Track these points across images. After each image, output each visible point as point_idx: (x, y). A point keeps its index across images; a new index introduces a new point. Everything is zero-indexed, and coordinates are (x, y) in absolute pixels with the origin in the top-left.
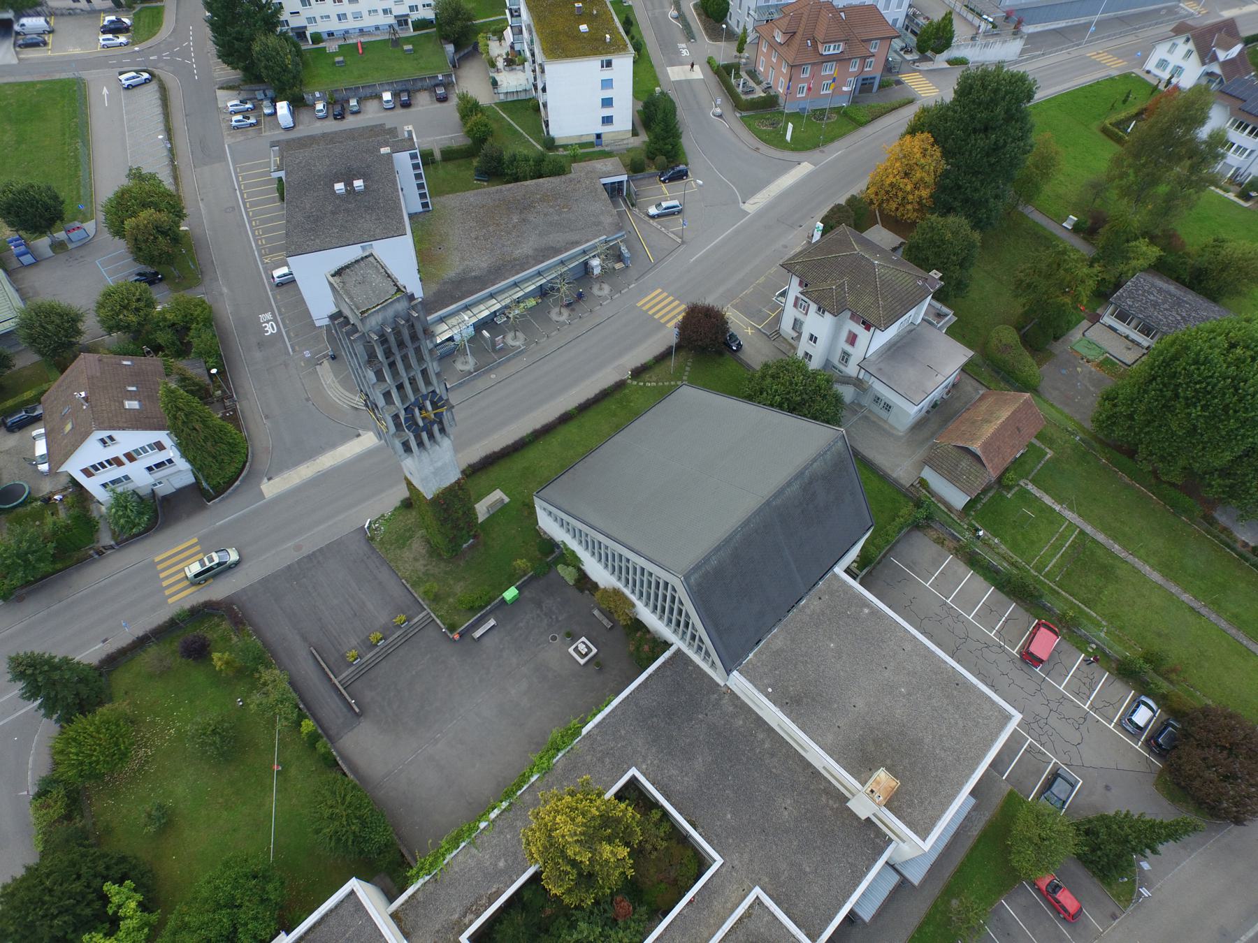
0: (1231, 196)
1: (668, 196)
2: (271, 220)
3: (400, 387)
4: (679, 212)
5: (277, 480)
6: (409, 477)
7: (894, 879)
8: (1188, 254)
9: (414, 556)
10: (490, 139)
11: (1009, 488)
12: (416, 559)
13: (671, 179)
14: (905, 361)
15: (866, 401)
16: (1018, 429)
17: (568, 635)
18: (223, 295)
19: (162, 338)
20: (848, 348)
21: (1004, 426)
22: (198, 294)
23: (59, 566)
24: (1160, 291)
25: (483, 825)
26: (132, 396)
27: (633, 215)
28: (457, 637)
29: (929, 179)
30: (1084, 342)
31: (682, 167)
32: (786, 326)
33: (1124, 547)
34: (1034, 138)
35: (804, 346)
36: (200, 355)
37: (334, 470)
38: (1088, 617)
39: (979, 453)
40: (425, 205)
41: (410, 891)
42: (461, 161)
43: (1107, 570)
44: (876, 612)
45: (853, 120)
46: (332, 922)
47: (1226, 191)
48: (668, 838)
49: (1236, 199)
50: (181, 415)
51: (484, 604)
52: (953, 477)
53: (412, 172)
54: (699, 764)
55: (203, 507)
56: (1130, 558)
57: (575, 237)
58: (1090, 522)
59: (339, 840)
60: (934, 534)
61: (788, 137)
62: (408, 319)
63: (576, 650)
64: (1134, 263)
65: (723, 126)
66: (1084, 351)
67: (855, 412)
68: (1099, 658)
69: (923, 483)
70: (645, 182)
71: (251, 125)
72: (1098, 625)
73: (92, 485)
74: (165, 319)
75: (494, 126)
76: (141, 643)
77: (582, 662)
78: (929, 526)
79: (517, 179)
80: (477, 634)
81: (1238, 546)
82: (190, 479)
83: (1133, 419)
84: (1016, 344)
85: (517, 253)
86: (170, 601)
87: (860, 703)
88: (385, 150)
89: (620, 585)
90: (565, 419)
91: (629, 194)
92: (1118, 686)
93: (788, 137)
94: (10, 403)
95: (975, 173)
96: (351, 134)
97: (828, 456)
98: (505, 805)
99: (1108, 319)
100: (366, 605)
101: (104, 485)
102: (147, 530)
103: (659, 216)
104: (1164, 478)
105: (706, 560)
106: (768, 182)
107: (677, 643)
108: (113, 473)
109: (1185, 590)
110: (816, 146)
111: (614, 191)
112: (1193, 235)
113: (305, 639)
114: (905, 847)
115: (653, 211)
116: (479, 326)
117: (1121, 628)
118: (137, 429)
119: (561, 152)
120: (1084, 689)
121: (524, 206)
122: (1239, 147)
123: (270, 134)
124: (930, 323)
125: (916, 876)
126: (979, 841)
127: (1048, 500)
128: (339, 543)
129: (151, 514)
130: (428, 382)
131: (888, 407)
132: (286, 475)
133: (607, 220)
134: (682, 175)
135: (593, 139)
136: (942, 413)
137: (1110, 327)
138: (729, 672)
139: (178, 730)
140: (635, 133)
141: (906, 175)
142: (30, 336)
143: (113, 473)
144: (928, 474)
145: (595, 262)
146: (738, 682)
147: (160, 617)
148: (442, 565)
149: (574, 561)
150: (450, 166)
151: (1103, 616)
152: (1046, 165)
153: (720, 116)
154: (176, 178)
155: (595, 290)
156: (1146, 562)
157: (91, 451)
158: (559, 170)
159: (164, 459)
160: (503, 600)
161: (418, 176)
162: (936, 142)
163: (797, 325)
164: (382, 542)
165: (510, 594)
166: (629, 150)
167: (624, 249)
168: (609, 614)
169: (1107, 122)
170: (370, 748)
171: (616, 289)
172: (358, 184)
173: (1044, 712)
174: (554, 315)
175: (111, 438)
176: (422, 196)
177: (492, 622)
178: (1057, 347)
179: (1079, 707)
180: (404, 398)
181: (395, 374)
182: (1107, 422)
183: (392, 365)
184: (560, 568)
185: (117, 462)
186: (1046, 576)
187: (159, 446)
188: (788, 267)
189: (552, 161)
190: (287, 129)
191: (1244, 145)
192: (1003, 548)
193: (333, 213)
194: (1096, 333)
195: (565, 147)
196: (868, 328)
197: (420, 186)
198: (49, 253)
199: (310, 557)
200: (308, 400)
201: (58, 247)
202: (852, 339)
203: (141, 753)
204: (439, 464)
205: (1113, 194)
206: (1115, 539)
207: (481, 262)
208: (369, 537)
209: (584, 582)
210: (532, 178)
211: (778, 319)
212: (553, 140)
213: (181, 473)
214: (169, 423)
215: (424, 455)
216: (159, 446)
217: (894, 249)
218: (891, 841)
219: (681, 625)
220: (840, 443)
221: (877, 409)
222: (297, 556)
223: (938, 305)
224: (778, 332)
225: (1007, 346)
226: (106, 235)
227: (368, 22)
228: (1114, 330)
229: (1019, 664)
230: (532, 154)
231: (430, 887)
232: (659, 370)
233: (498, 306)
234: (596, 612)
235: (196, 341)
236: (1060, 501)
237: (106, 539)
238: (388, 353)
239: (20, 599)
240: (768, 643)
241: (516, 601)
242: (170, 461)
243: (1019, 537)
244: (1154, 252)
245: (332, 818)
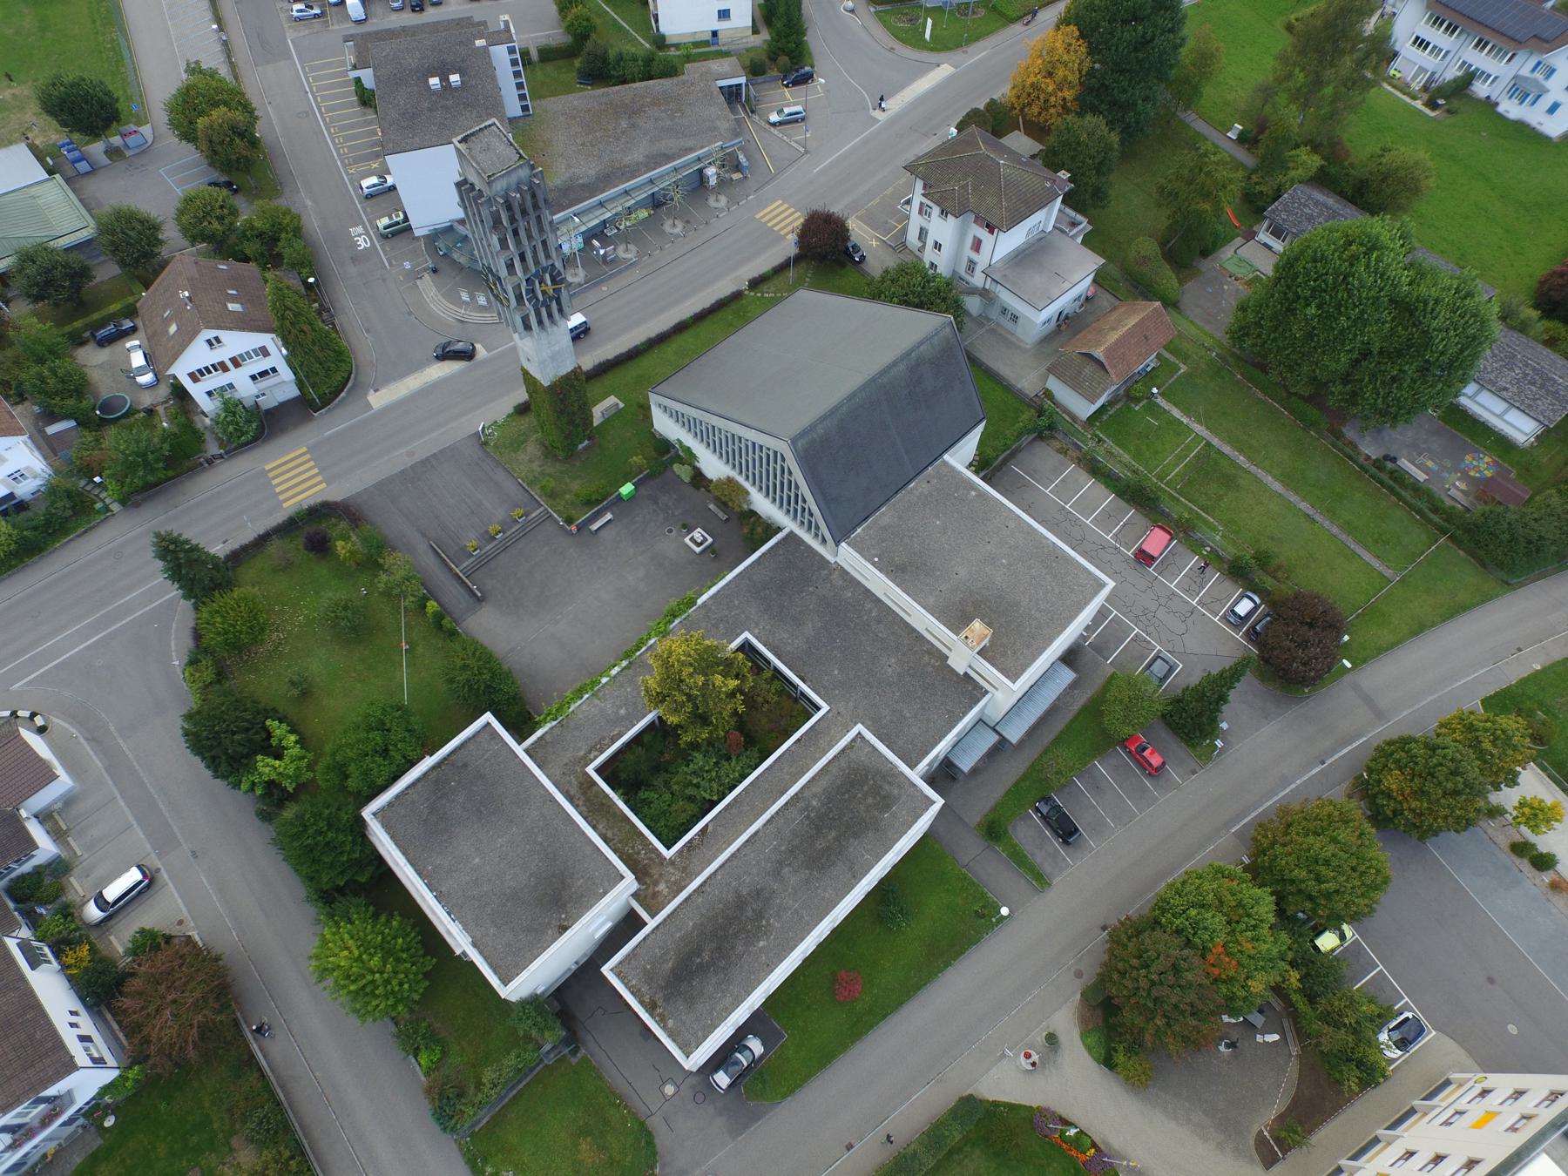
0: (1418, 104)
1: (791, 101)
2: (352, 126)
3: (522, 257)
5: (383, 391)
6: (526, 365)
8: (1352, 165)
9: (530, 456)
10: (594, 36)
11: (1137, 400)
12: (531, 461)
13: (795, 83)
14: (1034, 268)
15: (994, 314)
17: (684, 526)
18: (309, 205)
19: (251, 248)
20: (974, 256)
21: (1130, 333)
22: (282, 202)
23: (171, 473)
24: (1317, 203)
25: (604, 680)
26: (234, 299)
27: (753, 122)
28: (574, 528)
29: (1073, 78)
30: (1235, 260)
31: (807, 69)
32: (912, 237)
33: (1249, 459)
34: (1189, 30)
35: (929, 256)
36: (293, 266)
37: (431, 401)
38: (1205, 521)
39: (1102, 359)
40: (525, 108)
41: (539, 733)
42: (561, 63)
43: (1230, 480)
44: (982, 495)
45: (1002, 15)
46: (471, 747)
47: (1414, 98)
48: (780, 693)
49: (1423, 108)
50: (289, 314)
51: (597, 501)
52: (1076, 384)
53: (510, 70)
54: (808, 629)
55: (309, 418)
56: (1253, 469)
57: (690, 143)
58: (1217, 435)
59: (471, 689)
60: (1057, 444)
61: (927, 36)
62: (531, 186)
63: (692, 539)
64: (1292, 173)
65: (855, 22)
66: (1232, 268)
67: (982, 325)
68: (1212, 560)
69: (1048, 394)
70: (766, 86)
71: (316, 16)
72: (1215, 529)
73: (197, 391)
74: (252, 228)
75: (598, 21)
76: (262, 541)
77: (698, 550)
78: (1053, 437)
79: (624, 81)
80: (595, 527)
81: (1361, 459)
82: (294, 392)
83: (1261, 327)
84: (1158, 255)
85: (628, 159)
86: (285, 505)
87: (962, 572)
88: (480, 43)
89: (734, 474)
90: (680, 328)
91: (748, 99)
92: (1228, 584)
93: (927, 36)
94: (96, 316)
95: (1122, 72)
96: (434, 27)
98: (624, 663)
99: (1264, 237)
100: (488, 503)
101: (210, 393)
102: (255, 439)
103: (781, 123)
104: (1293, 390)
105: (813, 427)
106: (903, 87)
107: (789, 524)
108: (216, 380)
109: (1304, 499)
110: (958, 46)
111: (732, 94)
112: (1362, 143)
113: (424, 535)
114: (999, 695)
115: (774, 118)
116: (588, 236)
117: (1237, 532)
118: (243, 330)
119: (673, 52)
120: (1194, 587)
122: (1435, 47)
123: (338, 28)
124: (1063, 231)
125: (1014, 734)
126: (1079, 714)
127: (1176, 413)
128: (452, 448)
129: (255, 426)
130: (548, 256)
131: (1015, 318)
132: (393, 386)
133: (723, 126)
134: (806, 79)
135: (708, 37)
136: (1067, 324)
137: (1265, 245)
138: (837, 543)
139: (306, 616)
140: (755, 31)
141: (1050, 74)
142: (112, 243)
143: (216, 380)
144: (1053, 384)
145: (711, 171)
146: (847, 557)
147: (279, 518)
148: (558, 465)
149: (689, 457)
150: (549, 68)
151: (1220, 521)
152: (1205, 60)
153: (852, 11)
154: (236, 78)
155: (712, 202)
156: (1269, 472)
157: (197, 355)
158: (670, 71)
159: (267, 367)
160: (620, 497)
161: (517, 74)
162: (1082, 36)
163: (923, 233)
164: (496, 446)
165: (627, 489)
166: (747, 50)
167: (742, 158)
168: (723, 505)
169: (1293, 17)
170: (491, 628)
171: (733, 201)
172: (455, 78)
173: (1153, 606)
174: (667, 227)
175: (217, 339)
176: (522, 97)
177: (609, 516)
178: (1206, 265)
180: (526, 269)
181: (518, 243)
182: (1240, 333)
183: (516, 233)
184: (676, 467)
185: (222, 367)
187: (264, 352)
188: (911, 168)
189: (662, 61)
190: (358, 22)
191: (1440, 45)
192: (1126, 457)
193: (429, 110)
194: (1249, 251)
195: (677, 46)
196: (991, 232)
197: (520, 86)
198: (104, 160)
199: (424, 462)
200: (410, 313)
201: (114, 153)
202: (977, 246)
203: (274, 636)
204: (556, 348)
205: (1282, 99)
206: (1241, 451)
207: (588, 170)
208: (482, 441)
209: (699, 478)
210: (641, 80)
211: (904, 231)
212: (663, 37)
213: (284, 386)
214: (276, 324)
215: (543, 335)
216: (264, 352)
217: (1033, 157)
218: (987, 692)
219: (791, 504)
220: (948, 330)
221: (1006, 322)
222: (410, 462)
223: (1072, 213)
224: (904, 244)
225: (1145, 260)
226: (172, 140)
228: (1269, 248)
229: (1133, 564)
230: (640, 53)
231: (557, 731)
232: (778, 281)
233: (608, 215)
234: (712, 506)
235: (287, 252)
236: (1187, 411)
237: (213, 449)
238: (512, 220)
239: (137, 505)
240: (875, 522)
241: (632, 498)
242: (274, 370)
244: (1316, 161)
245: (465, 667)
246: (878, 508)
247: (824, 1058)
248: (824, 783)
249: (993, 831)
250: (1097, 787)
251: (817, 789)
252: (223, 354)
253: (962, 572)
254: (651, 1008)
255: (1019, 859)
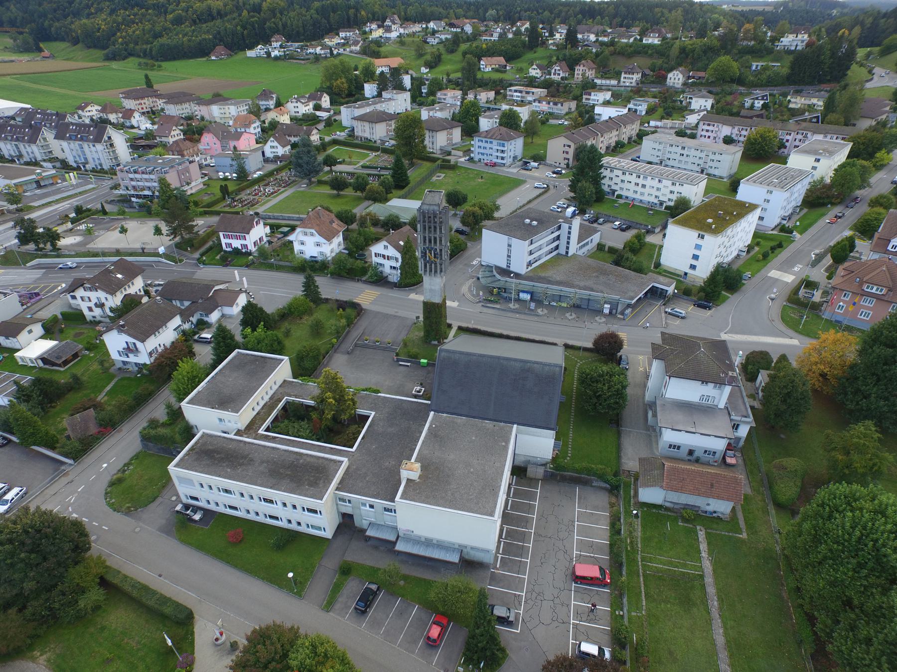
4: (683, 318)
7: (392, 538)
16: (712, 485)
54: (390, 430)
97: (547, 368)
103: (670, 314)
106: (755, 334)
121: (604, 273)
129: (380, 280)
151: (648, 610)
179: (569, 617)
186: (642, 565)
187: (397, 259)
227: (646, 198)
236: (710, 553)
243: (656, 540)
246: (461, 415)
247: (201, 547)
248: (312, 460)
249: (346, 570)
250: (401, 613)
251: (308, 459)
252: (386, 253)
253: (452, 457)
254: (192, 449)
255: (336, 589)
